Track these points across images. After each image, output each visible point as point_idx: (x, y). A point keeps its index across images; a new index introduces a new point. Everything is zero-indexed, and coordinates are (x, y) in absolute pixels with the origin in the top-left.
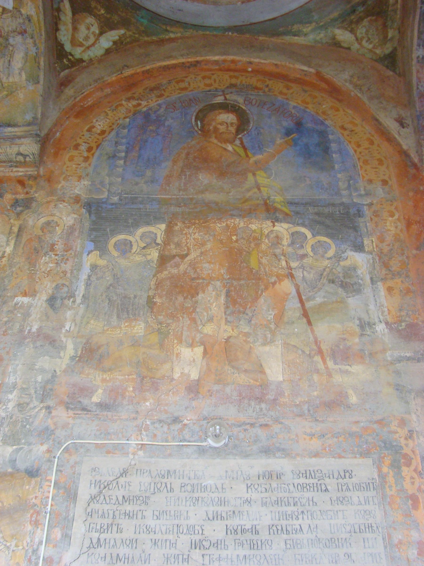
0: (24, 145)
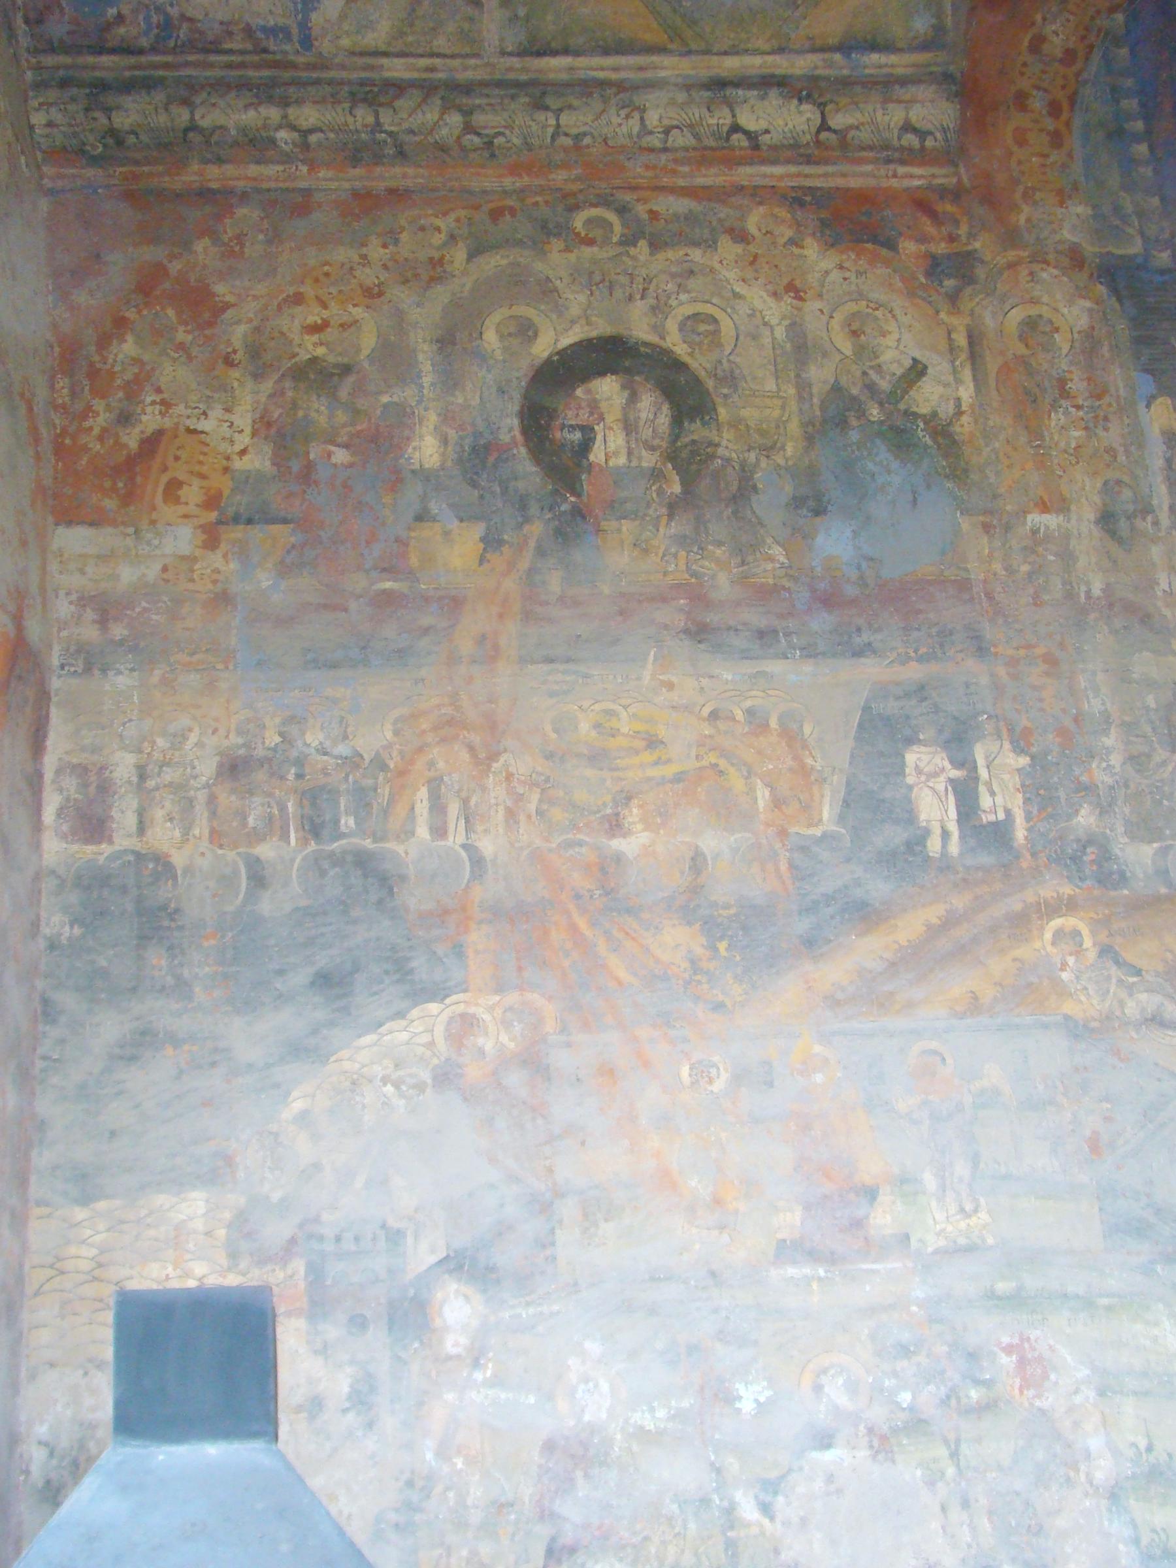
0: (918, 105)
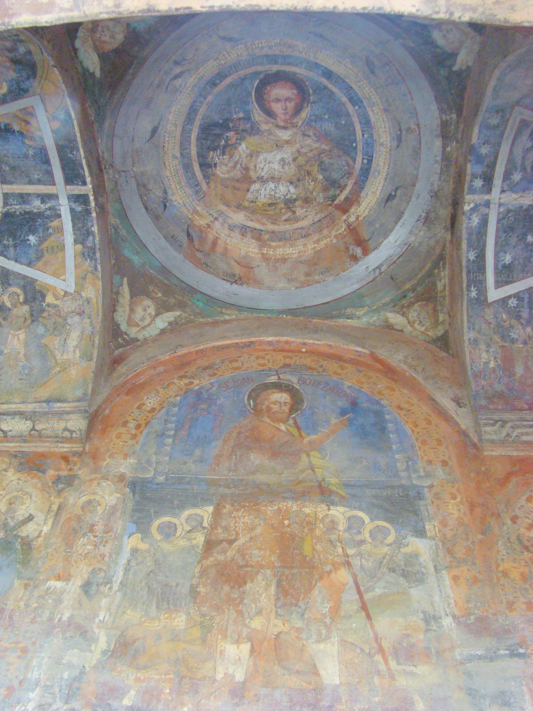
0: (71, 421)
